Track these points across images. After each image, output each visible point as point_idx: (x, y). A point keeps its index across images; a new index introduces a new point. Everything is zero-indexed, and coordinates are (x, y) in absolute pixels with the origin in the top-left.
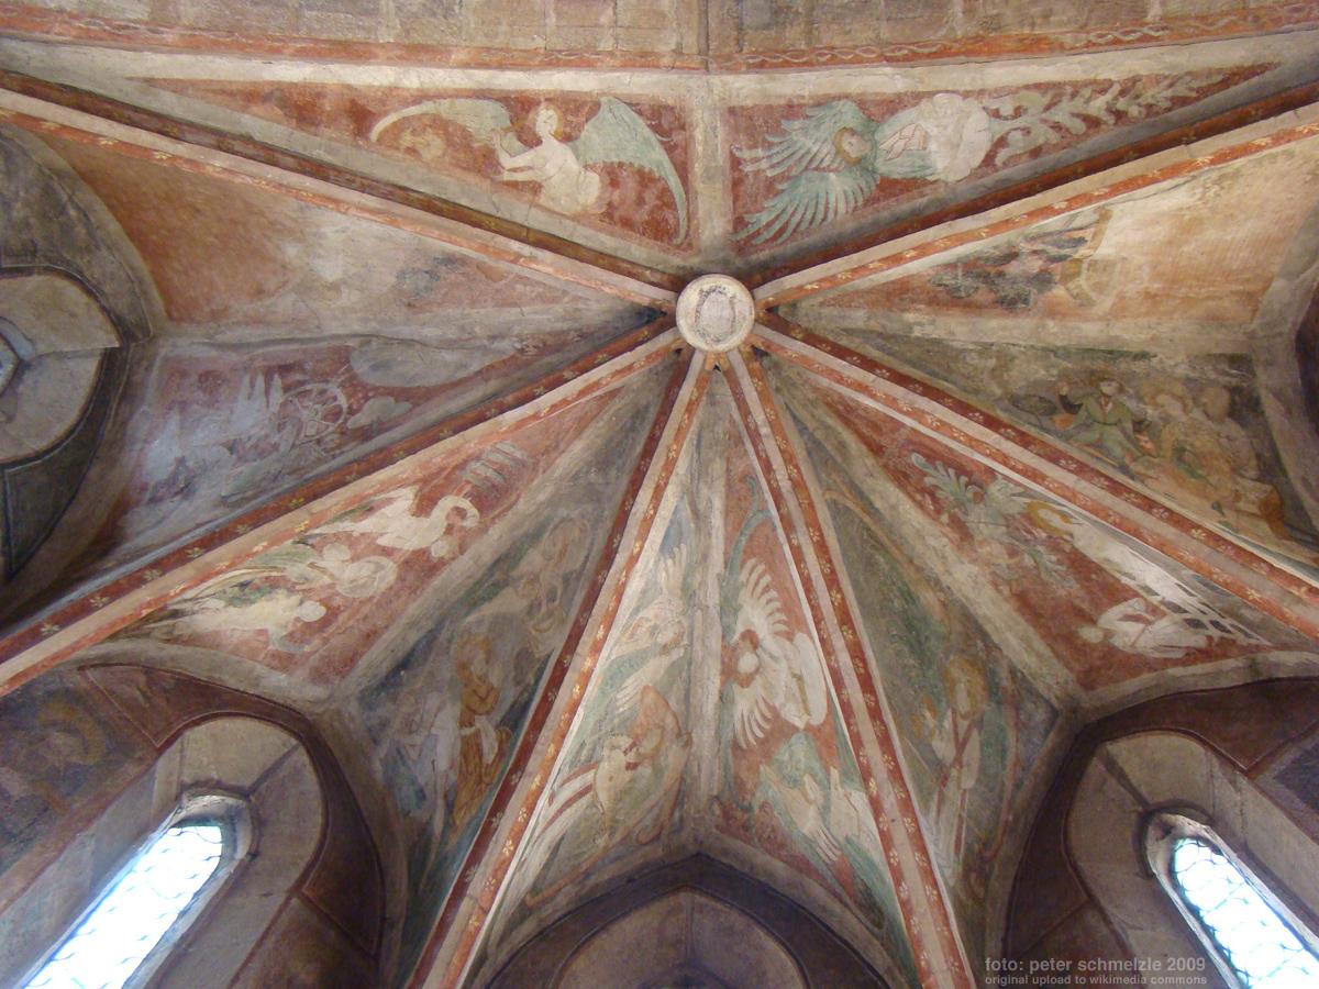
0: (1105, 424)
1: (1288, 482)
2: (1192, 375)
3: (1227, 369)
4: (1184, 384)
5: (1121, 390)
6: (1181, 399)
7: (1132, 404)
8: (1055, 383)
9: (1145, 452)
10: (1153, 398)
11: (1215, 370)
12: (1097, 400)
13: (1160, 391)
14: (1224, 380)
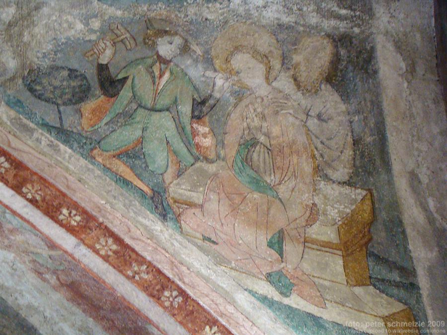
0: (153, 110)
1: (390, 183)
2: (286, 19)
3: (336, 8)
4: (274, 33)
5: (185, 49)
6: (264, 58)
7: (196, 72)
8: (95, 43)
9: (200, 155)
10: (227, 61)
11: (319, 10)
12: (149, 70)
13: (237, 49)
14: (329, 24)
